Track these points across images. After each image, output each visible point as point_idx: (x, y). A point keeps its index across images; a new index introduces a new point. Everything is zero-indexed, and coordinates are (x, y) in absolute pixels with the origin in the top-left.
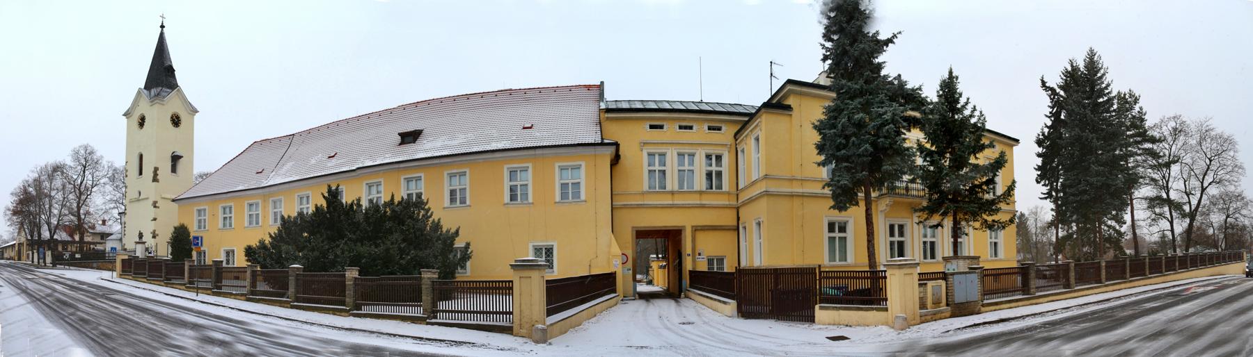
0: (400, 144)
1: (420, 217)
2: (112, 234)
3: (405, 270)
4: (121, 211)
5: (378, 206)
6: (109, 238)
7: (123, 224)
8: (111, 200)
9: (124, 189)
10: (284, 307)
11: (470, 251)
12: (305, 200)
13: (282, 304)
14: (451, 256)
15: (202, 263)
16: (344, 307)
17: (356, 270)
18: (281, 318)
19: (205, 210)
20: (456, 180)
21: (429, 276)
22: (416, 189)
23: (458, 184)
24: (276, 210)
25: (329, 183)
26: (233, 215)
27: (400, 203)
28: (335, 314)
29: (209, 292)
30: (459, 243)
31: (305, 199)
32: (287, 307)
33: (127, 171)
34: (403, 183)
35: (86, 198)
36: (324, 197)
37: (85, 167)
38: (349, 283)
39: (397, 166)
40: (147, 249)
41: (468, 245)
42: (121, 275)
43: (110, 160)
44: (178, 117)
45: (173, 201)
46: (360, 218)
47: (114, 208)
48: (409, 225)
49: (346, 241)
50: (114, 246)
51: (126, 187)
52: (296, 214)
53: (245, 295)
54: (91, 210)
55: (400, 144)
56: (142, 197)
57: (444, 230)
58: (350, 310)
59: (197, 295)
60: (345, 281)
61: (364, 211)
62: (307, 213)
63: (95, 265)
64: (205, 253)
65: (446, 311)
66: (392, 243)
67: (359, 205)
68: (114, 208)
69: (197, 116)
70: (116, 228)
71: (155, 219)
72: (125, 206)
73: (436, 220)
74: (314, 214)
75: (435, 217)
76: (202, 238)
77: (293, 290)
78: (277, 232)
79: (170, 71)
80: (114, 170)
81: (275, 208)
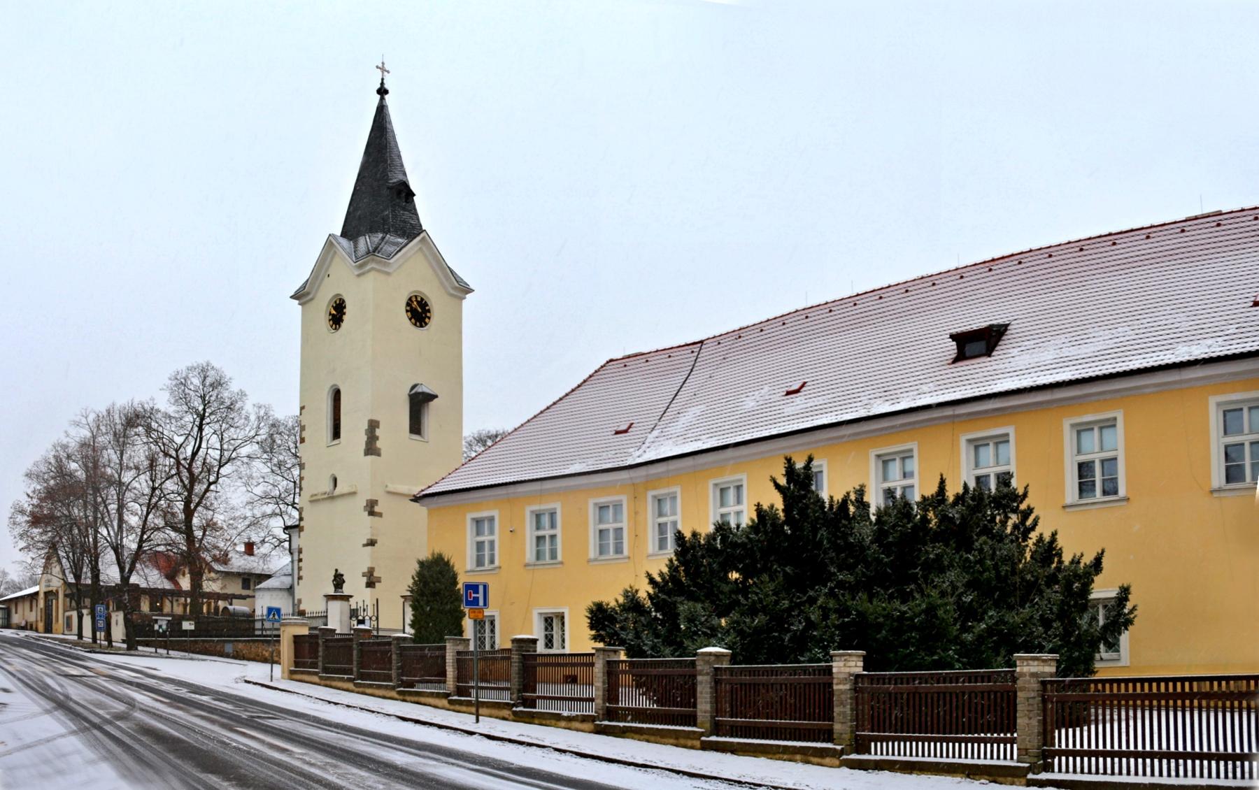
0: (955, 361)
1: (1009, 530)
2: (269, 577)
3: (974, 655)
4: (289, 523)
5: (907, 505)
6: (263, 585)
7: (296, 554)
8: (266, 497)
9: (296, 472)
10: (685, 746)
11: (1129, 606)
12: (731, 494)
13: (679, 740)
14: (1083, 622)
15: (488, 648)
16: (830, 745)
17: (858, 656)
18: (678, 772)
19: (491, 519)
20: (1091, 440)
21: (1033, 670)
22: (997, 464)
23: (1097, 449)
24: (662, 520)
25: (788, 453)
26: (558, 531)
27: (959, 499)
28: (808, 762)
29: (506, 713)
30: (1102, 589)
31: (731, 494)
32: (692, 748)
33: (303, 428)
34: (965, 452)
35: (207, 490)
36: (777, 486)
37: (202, 418)
38: (841, 687)
39: (948, 412)
40: (354, 613)
41: (1125, 592)
42: (292, 672)
43: (262, 403)
44: (423, 304)
45: (416, 499)
46: (865, 532)
47: (274, 514)
48: (981, 550)
49: (831, 589)
50: (275, 604)
51: (302, 466)
52: (711, 529)
53: (591, 719)
54: (219, 518)
55: (955, 361)
56: (338, 491)
57: (1067, 559)
58: (842, 752)
59: (477, 721)
60: (831, 685)
61: (873, 518)
62: (738, 526)
63: (229, 648)
64: (492, 623)
65: (1074, 754)
66: (943, 594)
67: (862, 505)
68: (274, 514)
69: (469, 302)
70: (280, 561)
71: (372, 543)
72: (300, 511)
73: (1047, 538)
74: (754, 528)
75: (1044, 530)
76: (485, 587)
77: (708, 707)
78: (665, 570)
79: (405, 193)
80: (273, 425)
81: (661, 515)
